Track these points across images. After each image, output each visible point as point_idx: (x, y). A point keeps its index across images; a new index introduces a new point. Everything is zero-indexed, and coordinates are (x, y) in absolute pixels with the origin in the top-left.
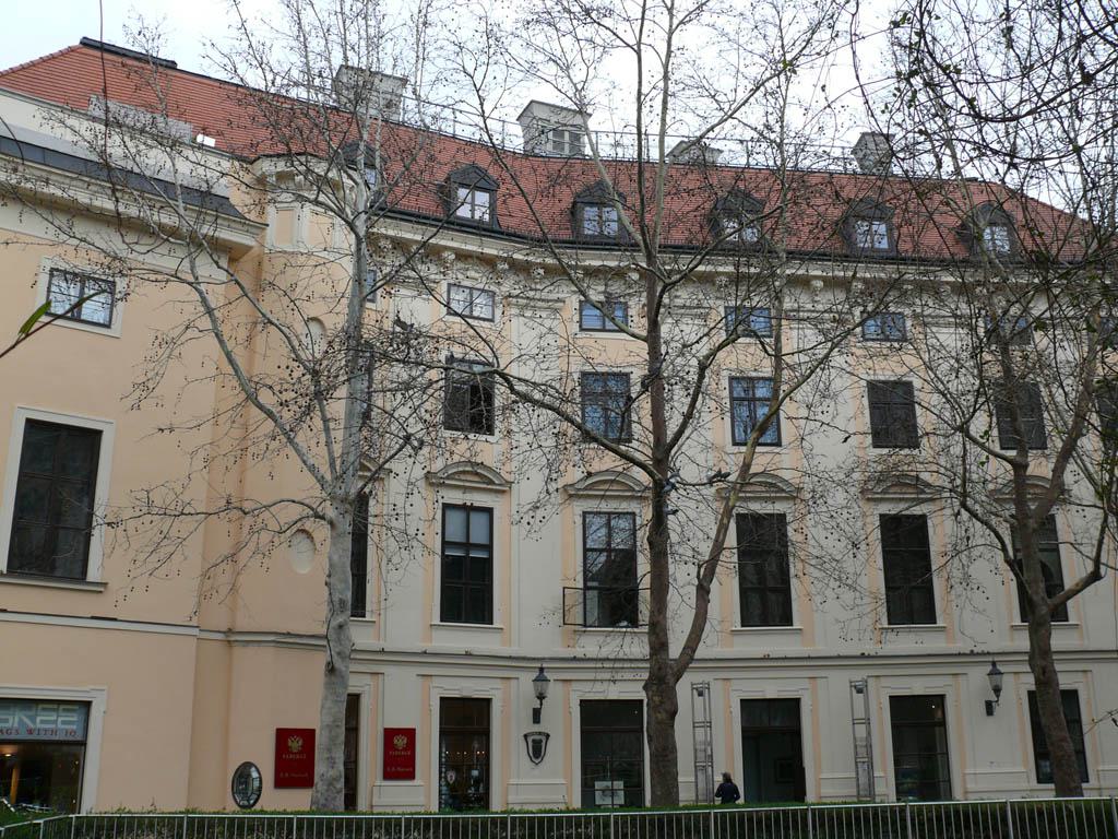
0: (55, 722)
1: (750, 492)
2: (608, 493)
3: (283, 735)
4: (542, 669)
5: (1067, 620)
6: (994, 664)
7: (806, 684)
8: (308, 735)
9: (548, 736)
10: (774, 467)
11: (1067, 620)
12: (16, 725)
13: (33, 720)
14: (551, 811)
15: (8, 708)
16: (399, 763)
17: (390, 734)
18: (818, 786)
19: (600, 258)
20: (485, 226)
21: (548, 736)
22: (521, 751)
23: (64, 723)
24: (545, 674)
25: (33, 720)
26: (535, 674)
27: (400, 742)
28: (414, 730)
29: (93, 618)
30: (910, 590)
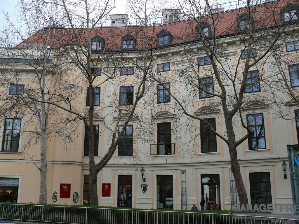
0: (13, 182)
1: (161, 117)
2: (166, 117)
3: (62, 185)
4: (143, 167)
5: (217, 151)
6: (284, 161)
7: (221, 170)
8: (109, 185)
9: (147, 185)
10: (43, 121)
11: (217, 151)
12: (5, 183)
13: (9, 182)
14: (103, 207)
15: (3, 180)
16: (106, 192)
17: (104, 185)
18: (224, 202)
19: (164, 51)
20: (126, 50)
21: (147, 185)
22: (140, 189)
23: (15, 183)
24: (285, 162)
25: (9, 182)
26: (282, 163)
27: (107, 187)
28: (110, 184)
29: (19, 160)
30: (208, 141)
